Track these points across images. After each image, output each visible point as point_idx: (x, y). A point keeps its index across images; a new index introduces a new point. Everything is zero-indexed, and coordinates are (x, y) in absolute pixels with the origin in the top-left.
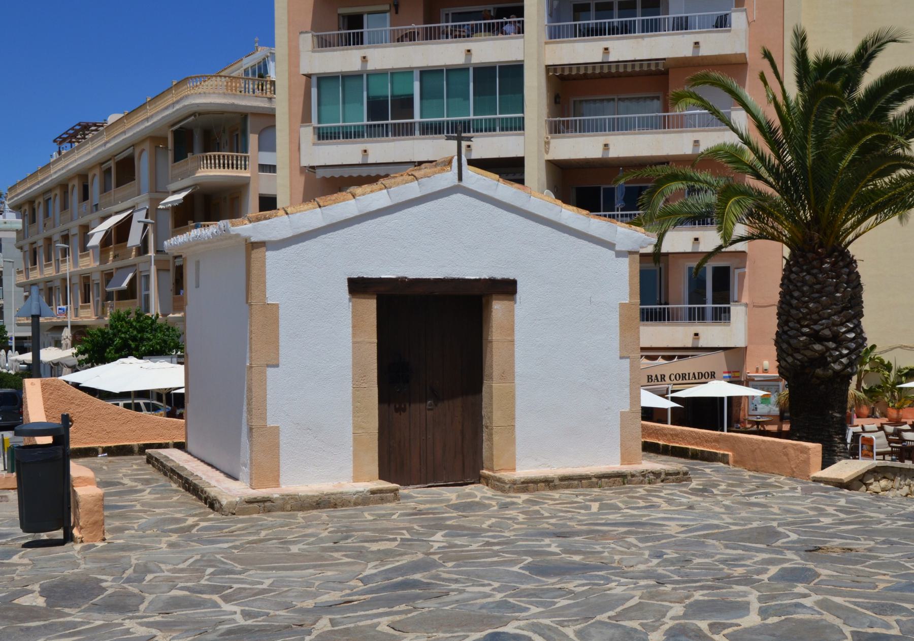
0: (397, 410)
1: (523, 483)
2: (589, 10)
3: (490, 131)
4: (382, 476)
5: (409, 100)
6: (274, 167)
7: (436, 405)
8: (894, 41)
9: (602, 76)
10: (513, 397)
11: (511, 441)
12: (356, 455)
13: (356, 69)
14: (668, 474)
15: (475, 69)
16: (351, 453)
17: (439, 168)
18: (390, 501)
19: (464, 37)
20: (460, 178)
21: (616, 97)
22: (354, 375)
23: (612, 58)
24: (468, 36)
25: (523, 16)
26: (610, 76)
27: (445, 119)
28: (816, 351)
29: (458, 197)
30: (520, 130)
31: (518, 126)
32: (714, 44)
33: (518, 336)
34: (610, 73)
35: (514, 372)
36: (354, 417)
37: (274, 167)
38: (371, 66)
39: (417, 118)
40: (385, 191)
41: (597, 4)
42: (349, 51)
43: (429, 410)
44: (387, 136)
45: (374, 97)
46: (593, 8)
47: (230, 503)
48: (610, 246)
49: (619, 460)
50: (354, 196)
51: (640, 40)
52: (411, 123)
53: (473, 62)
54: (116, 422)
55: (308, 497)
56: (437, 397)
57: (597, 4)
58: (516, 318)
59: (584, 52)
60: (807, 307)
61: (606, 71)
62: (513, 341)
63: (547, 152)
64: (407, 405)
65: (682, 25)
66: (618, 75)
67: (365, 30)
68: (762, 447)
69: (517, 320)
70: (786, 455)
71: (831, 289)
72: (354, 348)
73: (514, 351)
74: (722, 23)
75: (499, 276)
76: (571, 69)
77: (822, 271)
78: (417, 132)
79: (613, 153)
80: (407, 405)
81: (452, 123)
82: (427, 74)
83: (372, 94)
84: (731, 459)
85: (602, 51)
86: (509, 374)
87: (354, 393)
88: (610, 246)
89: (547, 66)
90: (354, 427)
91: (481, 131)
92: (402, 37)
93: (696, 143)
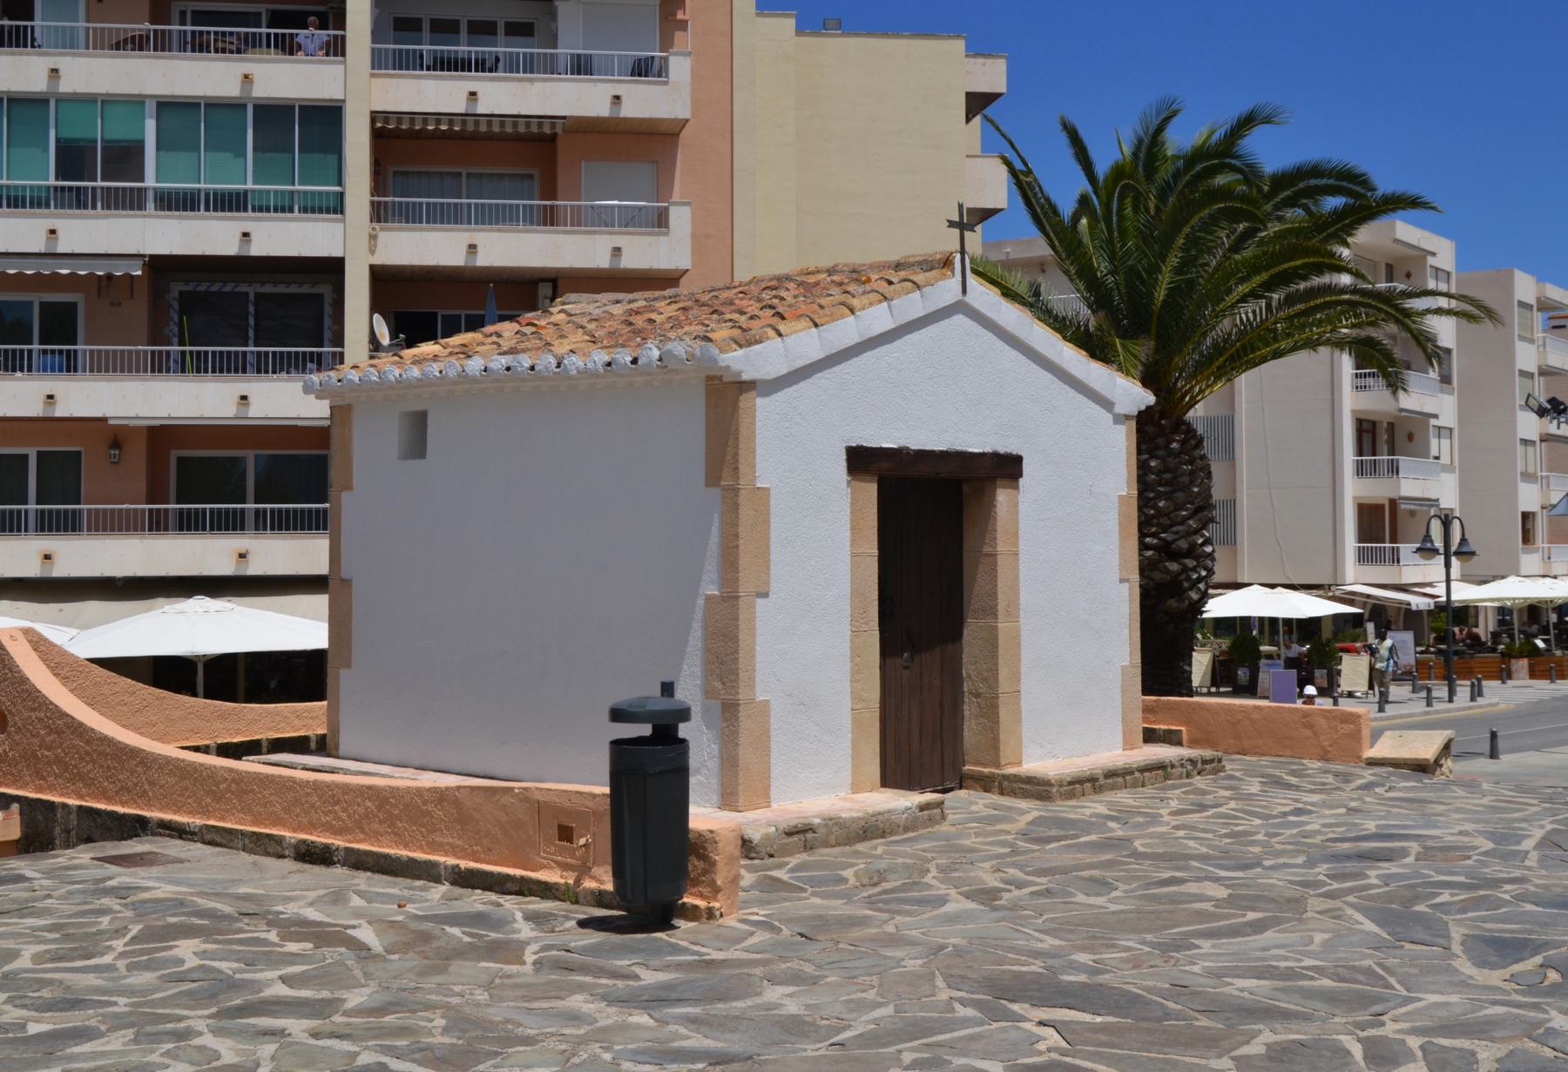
1: (1070, 783)
2: (420, 30)
3: (283, 211)
4: (889, 779)
5: (137, 148)
8: (1167, 120)
9: (461, 136)
11: (1017, 719)
12: (854, 746)
13: (38, 89)
14: (1205, 762)
15: (256, 107)
17: (934, 272)
19: (231, 52)
20: (964, 291)
21: (464, 171)
22: (853, 609)
23: (482, 108)
24: (239, 51)
25: (344, 29)
26: (475, 137)
27: (202, 186)
28: (1168, 572)
29: (959, 319)
30: (335, 212)
31: (335, 206)
32: (643, 102)
34: (423, 130)
38: (66, 86)
39: (150, 181)
40: (885, 304)
41: (469, 22)
42: (25, 58)
44: (94, 207)
45: (67, 140)
46: (426, 26)
47: (767, 837)
48: (1106, 404)
49: (1120, 745)
50: (852, 311)
51: (526, 84)
52: (140, 189)
53: (254, 94)
54: (125, 709)
55: (853, 820)
57: (469, 22)
59: (434, 95)
60: (1155, 507)
61: (470, 127)
63: (372, 252)
65: (581, 66)
66: (489, 137)
67: (37, 23)
68: (1255, 716)
70: (1310, 726)
71: (1185, 479)
72: (852, 564)
74: (642, 69)
75: (1002, 450)
76: (412, 121)
77: (1171, 453)
78: (150, 205)
79: (484, 260)
81: (215, 194)
82: (169, 108)
83: (107, 137)
84: (1185, 737)
85: (465, 95)
88: (1106, 404)
89: (373, 112)
91: (268, 210)
92: (125, 40)
93: (617, 251)
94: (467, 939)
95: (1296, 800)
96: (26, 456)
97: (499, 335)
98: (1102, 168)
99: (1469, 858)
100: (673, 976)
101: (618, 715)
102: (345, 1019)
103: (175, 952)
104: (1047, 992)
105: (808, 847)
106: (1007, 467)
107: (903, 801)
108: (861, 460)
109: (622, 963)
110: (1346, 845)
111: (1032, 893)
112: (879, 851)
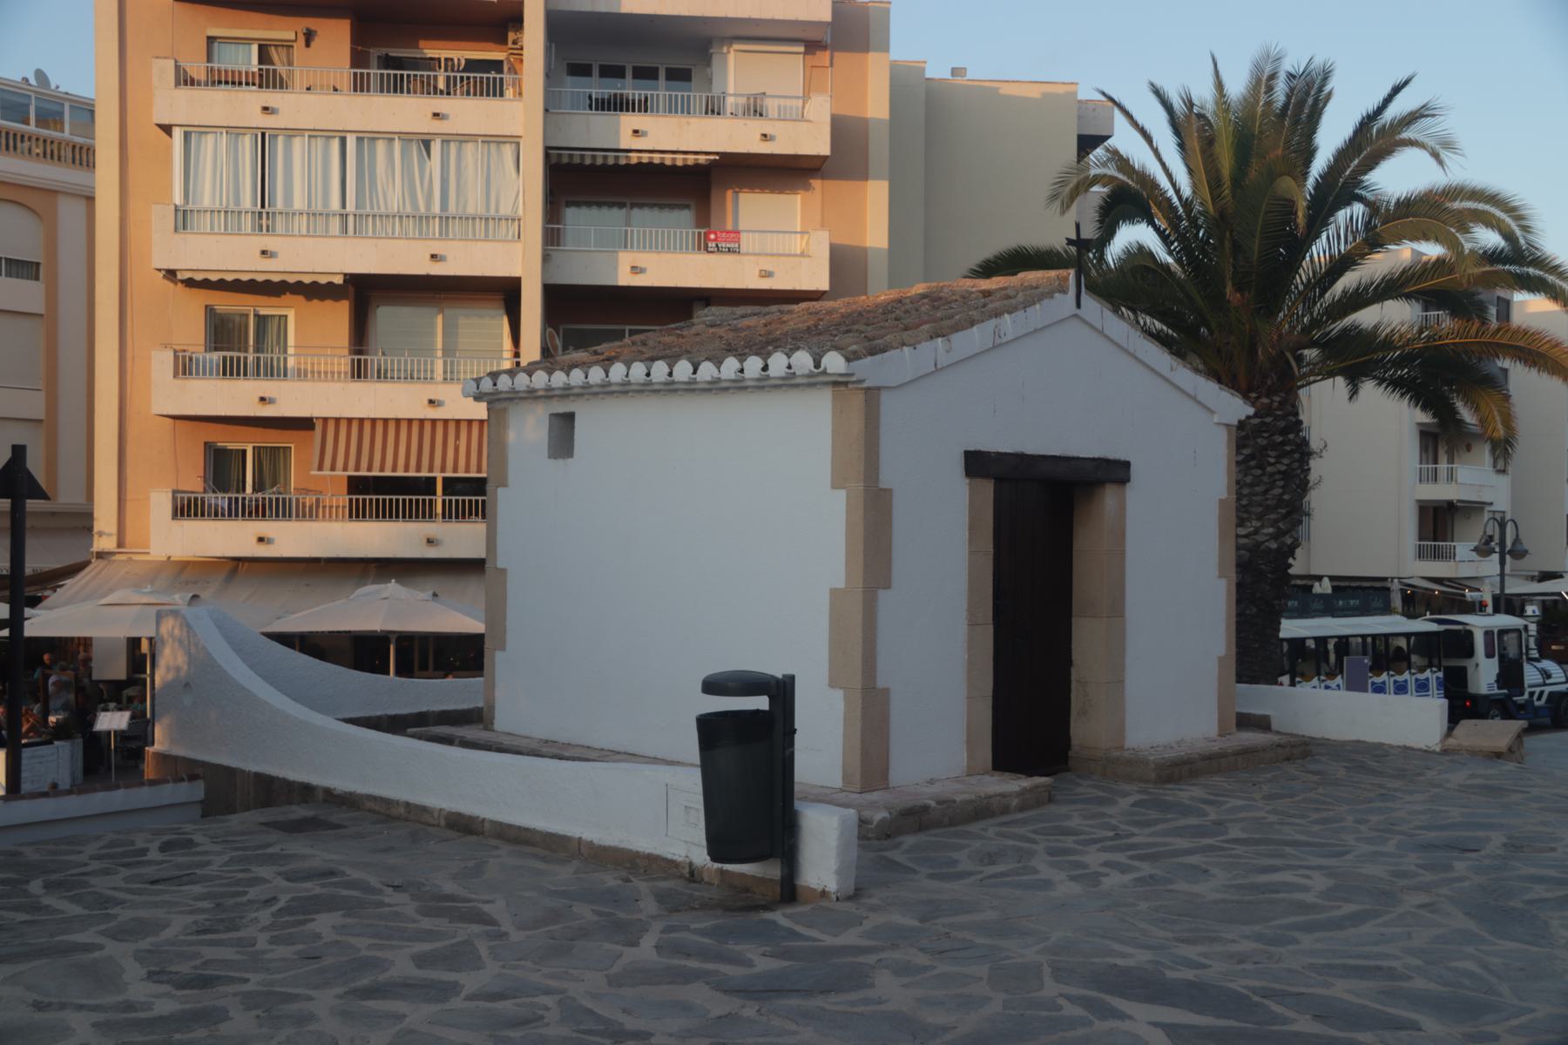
94: (595, 918)
95: (1381, 786)
96: (244, 452)
97: (644, 344)
98: (1522, 380)
99: (1553, 850)
100: (786, 964)
101: (712, 686)
102: (468, 1004)
103: (310, 926)
104: (1151, 988)
105: (921, 828)
106: (1116, 472)
107: (1013, 785)
108: (977, 463)
109: (733, 947)
110: (1433, 834)
111: (1137, 880)
112: (991, 832)
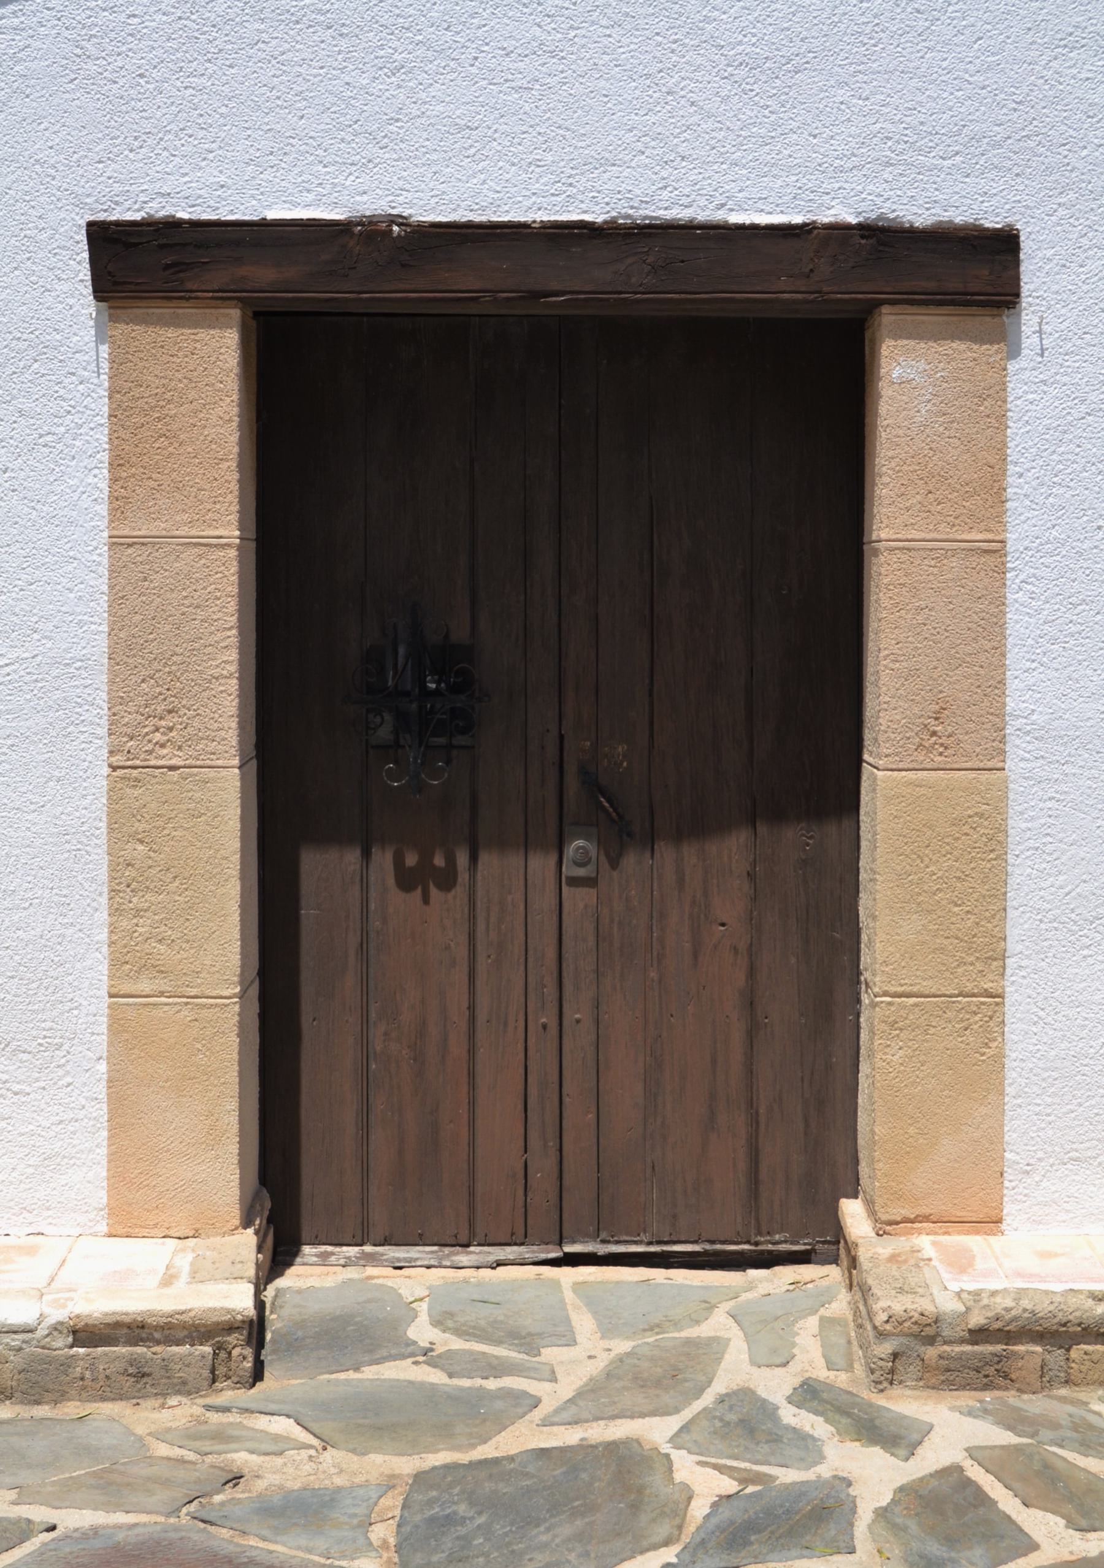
0: (406, 880)
1: (979, 1335)
6: (1004, 245)
7: (614, 864)
10: (995, 844)
11: (981, 1072)
16: (101, 1090)
18: (184, 1388)
22: (116, 702)
33: (1022, 528)
35: (1000, 713)
36: (116, 911)
37: (1004, 245)
43: (574, 882)
56: (624, 823)
58: (1014, 429)
62: (996, 551)
64: (462, 859)
69: (1020, 438)
73: (1001, 602)
75: (917, 210)
80: (462, 859)
86: (971, 729)
87: (114, 796)
90: (116, 963)
